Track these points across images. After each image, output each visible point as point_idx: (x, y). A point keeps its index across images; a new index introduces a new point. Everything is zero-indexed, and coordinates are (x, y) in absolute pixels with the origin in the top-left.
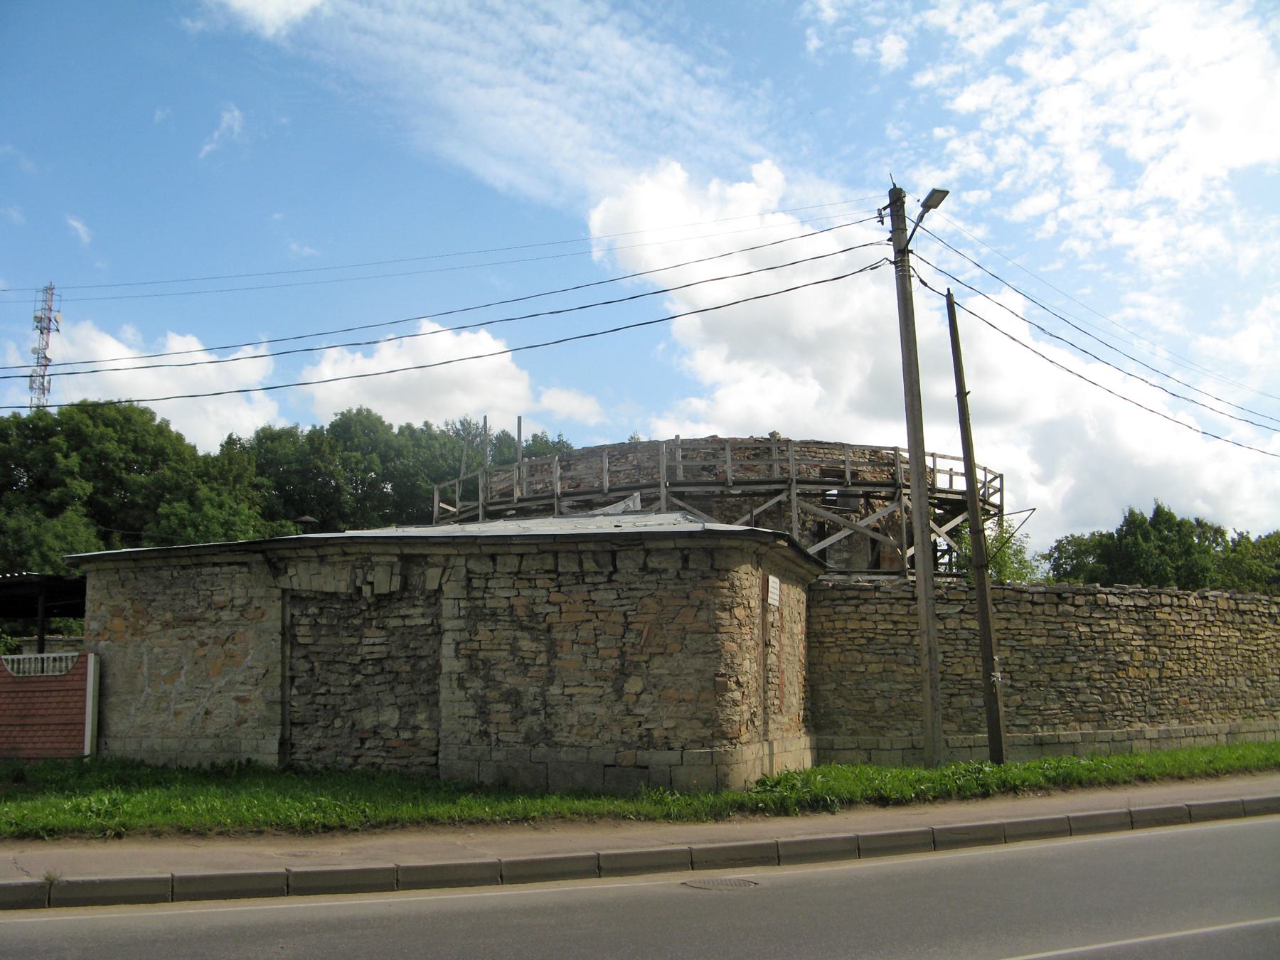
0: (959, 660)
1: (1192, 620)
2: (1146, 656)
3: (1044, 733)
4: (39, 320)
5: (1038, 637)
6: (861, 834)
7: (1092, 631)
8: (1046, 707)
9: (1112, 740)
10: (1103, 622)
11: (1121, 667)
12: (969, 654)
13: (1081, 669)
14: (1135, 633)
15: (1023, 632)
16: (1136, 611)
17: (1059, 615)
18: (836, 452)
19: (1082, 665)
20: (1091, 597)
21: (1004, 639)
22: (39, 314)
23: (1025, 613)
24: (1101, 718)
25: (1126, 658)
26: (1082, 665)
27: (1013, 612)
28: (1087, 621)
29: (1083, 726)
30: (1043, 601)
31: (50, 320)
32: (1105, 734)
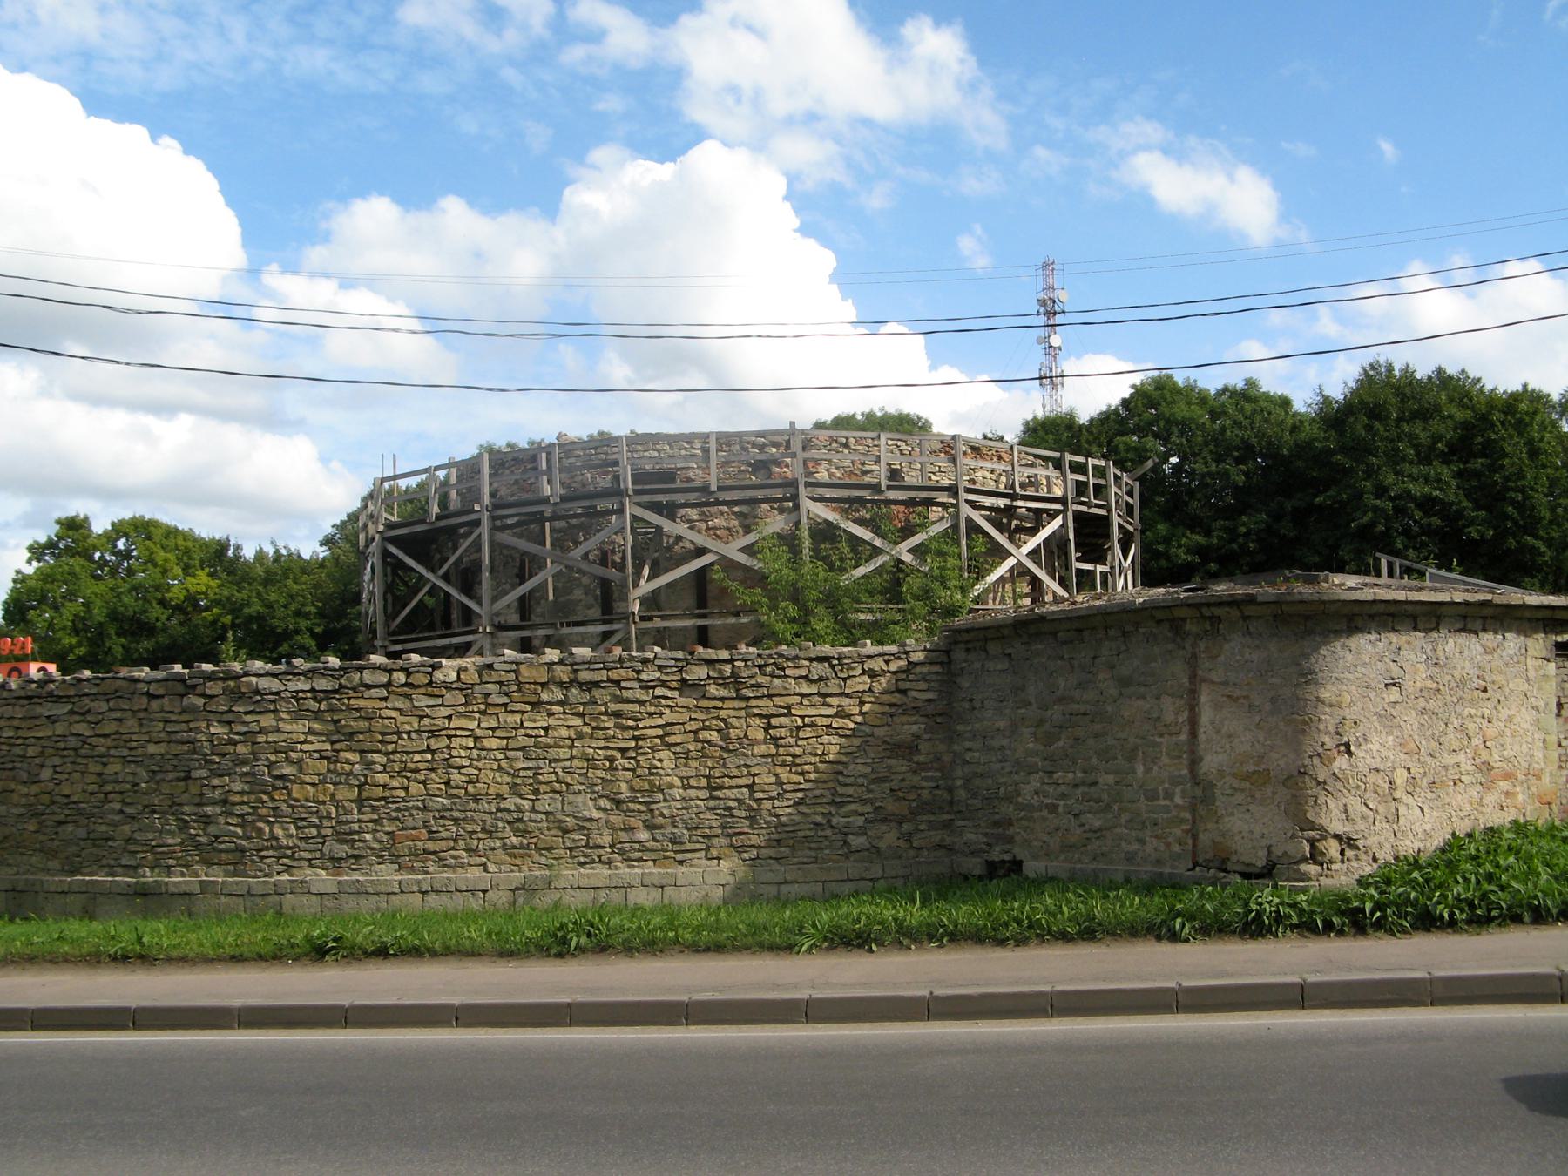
0: (66, 776)
1: (442, 705)
2: (332, 767)
3: (149, 876)
4: (1043, 302)
5: (156, 743)
6: (1312, 978)
7: (231, 731)
8: (160, 842)
9: (248, 892)
10: (248, 718)
11: (279, 783)
12: (78, 768)
13: (215, 787)
14: (311, 732)
15: (135, 737)
16: (315, 699)
17: (183, 711)
18: (640, 448)
19: (216, 782)
20: (232, 683)
21: (116, 748)
22: (1041, 296)
23: (139, 710)
24: (238, 859)
25: (288, 770)
26: (216, 782)
27: (125, 710)
28: (226, 718)
29: (210, 870)
30: (161, 692)
31: (1054, 302)
32: (237, 883)
